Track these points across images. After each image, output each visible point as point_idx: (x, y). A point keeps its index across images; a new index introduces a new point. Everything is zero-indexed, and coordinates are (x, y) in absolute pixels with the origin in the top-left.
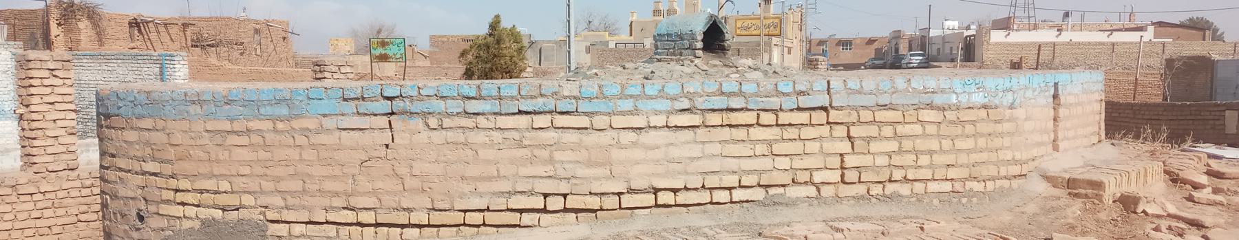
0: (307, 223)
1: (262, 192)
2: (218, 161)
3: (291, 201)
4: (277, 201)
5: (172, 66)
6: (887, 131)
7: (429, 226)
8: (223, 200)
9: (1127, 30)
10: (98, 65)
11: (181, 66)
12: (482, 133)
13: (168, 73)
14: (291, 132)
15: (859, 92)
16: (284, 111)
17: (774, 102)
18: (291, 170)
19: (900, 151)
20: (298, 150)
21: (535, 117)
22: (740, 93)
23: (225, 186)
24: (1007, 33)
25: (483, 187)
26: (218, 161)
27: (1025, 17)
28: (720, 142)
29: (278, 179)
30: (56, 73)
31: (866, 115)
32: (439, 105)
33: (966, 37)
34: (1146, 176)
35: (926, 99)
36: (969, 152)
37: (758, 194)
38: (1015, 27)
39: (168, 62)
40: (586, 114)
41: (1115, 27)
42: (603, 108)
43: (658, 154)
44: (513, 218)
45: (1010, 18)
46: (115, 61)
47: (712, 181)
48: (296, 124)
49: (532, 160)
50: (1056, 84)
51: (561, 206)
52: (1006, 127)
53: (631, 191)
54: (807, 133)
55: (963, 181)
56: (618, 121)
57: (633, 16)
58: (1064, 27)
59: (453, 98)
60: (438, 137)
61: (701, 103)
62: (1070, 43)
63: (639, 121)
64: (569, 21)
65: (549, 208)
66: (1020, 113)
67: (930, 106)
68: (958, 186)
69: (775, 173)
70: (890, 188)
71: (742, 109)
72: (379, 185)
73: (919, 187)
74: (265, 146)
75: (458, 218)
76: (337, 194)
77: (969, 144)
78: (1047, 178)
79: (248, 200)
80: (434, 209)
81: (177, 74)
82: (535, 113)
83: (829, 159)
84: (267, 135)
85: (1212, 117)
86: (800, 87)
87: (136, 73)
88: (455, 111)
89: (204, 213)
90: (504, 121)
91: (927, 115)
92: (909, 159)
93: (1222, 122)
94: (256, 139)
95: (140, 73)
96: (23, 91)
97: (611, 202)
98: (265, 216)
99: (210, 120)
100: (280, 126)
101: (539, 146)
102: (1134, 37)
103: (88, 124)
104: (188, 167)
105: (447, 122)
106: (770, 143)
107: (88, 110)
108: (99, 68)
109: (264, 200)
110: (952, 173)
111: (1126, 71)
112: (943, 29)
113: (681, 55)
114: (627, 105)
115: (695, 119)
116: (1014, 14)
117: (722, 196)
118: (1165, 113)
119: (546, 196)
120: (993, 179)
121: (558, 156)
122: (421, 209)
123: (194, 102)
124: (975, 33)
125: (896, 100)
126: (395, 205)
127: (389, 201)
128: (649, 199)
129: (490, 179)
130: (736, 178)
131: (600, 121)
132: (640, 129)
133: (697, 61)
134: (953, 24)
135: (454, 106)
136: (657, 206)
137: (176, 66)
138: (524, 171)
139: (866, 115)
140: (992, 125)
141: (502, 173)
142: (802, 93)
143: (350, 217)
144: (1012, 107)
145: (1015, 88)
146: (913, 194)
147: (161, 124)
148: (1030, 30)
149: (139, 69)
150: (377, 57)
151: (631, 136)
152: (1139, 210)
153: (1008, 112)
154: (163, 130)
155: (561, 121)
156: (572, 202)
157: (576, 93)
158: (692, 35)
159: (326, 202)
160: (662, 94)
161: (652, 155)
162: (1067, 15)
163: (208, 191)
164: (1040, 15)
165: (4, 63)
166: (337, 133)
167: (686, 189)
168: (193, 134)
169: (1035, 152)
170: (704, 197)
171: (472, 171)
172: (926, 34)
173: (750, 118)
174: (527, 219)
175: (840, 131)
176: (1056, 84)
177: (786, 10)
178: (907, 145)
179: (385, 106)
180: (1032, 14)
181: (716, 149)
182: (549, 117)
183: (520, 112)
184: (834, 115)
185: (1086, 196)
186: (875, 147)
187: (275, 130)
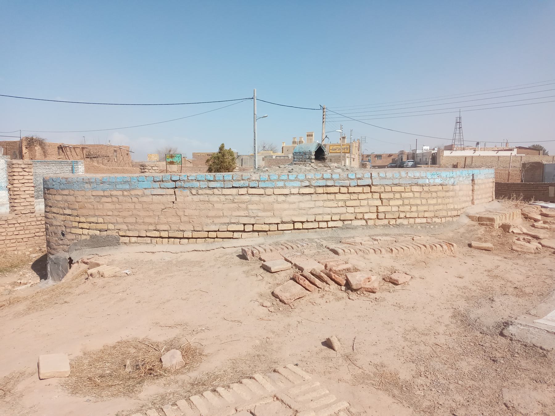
0: (137, 237)
1: (117, 223)
2: (98, 209)
3: (130, 227)
4: (124, 227)
5: (77, 167)
6: (398, 196)
7: (192, 238)
9: (505, 150)
11: (81, 166)
13: (75, 170)
16: (127, 187)
17: (347, 183)
18: (130, 213)
19: (403, 205)
20: (133, 204)
21: (240, 189)
22: (332, 179)
23: (101, 220)
25: (217, 221)
26: (98, 209)
28: (322, 201)
29: (124, 217)
30: (25, 170)
31: (388, 189)
32: (197, 184)
33: (433, 153)
35: (415, 181)
36: (434, 205)
37: (340, 224)
38: (455, 149)
40: (262, 188)
41: (499, 149)
42: (270, 185)
44: (230, 235)
45: (452, 145)
46: (51, 164)
48: (133, 192)
49: (239, 209)
52: (451, 194)
53: (283, 222)
54: (362, 196)
55: (432, 218)
56: (277, 191)
57: (283, 144)
58: (477, 149)
59: (203, 181)
60: (196, 198)
61: (314, 183)
62: (479, 156)
63: (286, 191)
64: (255, 147)
66: (457, 187)
67: (417, 184)
68: (429, 220)
69: (347, 214)
70: (399, 221)
72: (170, 220)
73: (412, 221)
74: (119, 203)
75: (205, 234)
76: (151, 224)
77: (434, 201)
79: (111, 226)
82: (240, 187)
83: (371, 208)
84: (120, 198)
86: (358, 176)
88: (204, 186)
89: (92, 232)
90: (226, 191)
91: (415, 188)
92: (407, 208)
95: (63, 170)
96: (11, 178)
100: (125, 193)
102: (508, 153)
103: (39, 192)
104: (84, 212)
105: (200, 192)
106: (345, 201)
107: (40, 186)
108: (44, 167)
109: (118, 227)
110: (426, 215)
111: (504, 169)
112: (422, 150)
114: (281, 184)
115: (311, 190)
118: (522, 188)
119: (244, 225)
120: (445, 217)
121: (250, 207)
122: (189, 231)
123: (87, 183)
124: (437, 152)
125: (401, 182)
126: (177, 229)
127: (174, 227)
129: (219, 217)
131: (269, 191)
132: (287, 195)
133: (312, 164)
135: (203, 185)
136: (294, 229)
137: (79, 167)
139: (388, 189)
140: (444, 193)
141: (225, 214)
142: (359, 179)
143: (157, 234)
144: (453, 185)
145: (455, 176)
147: (72, 192)
149: (62, 168)
151: (283, 198)
152: (510, 231)
153: (452, 187)
156: (256, 228)
157: (258, 179)
158: (310, 153)
159: (146, 227)
160: (297, 179)
161: (292, 206)
162: (478, 144)
163: (93, 223)
164: (466, 144)
166: (151, 197)
167: (307, 221)
168: (86, 197)
169: (464, 205)
170: (316, 225)
171: (212, 213)
173: (336, 190)
174: (236, 235)
175: (376, 196)
177: (352, 142)
178: (406, 202)
179: (173, 184)
180: (462, 143)
181: (321, 203)
182: (246, 189)
183: (233, 187)
184: (374, 189)
185: (487, 225)
186: (392, 203)
187: (123, 195)
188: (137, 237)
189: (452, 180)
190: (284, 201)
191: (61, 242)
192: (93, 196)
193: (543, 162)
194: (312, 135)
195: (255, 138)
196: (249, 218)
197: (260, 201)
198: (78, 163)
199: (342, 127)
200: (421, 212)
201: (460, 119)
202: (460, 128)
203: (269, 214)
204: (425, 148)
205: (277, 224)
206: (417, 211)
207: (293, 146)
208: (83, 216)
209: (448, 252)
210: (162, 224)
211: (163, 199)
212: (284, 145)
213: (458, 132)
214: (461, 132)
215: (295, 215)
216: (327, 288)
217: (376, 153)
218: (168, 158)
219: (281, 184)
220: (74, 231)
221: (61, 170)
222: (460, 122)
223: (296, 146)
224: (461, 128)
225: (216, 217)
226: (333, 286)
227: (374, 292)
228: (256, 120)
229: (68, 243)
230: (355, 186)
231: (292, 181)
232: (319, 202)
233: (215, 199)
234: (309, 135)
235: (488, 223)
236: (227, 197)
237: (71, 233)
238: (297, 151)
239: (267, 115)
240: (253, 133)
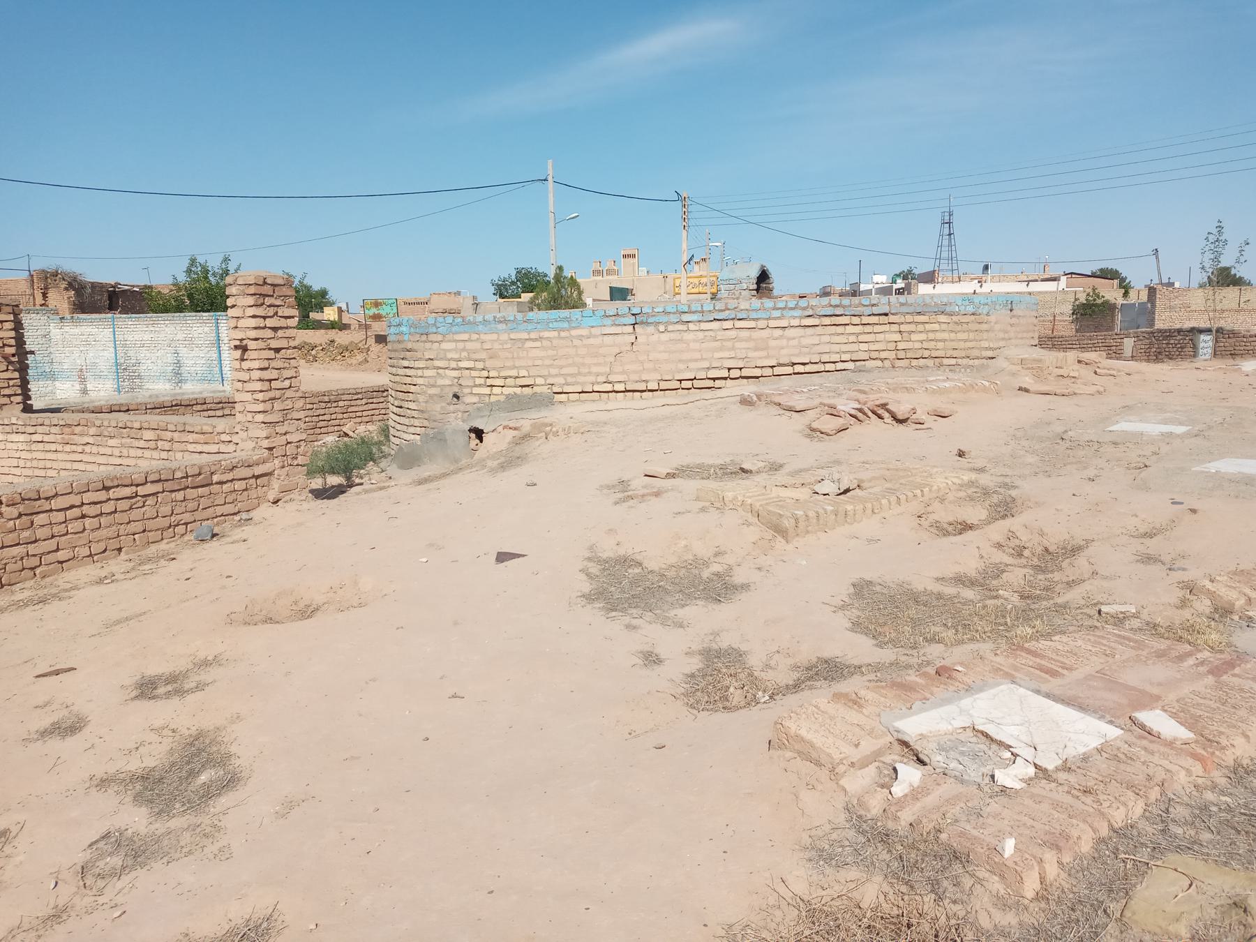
0: (580, 393)
1: (550, 375)
2: (519, 358)
3: (570, 380)
10: (145, 326)
14: (571, 338)
16: (566, 325)
24: (933, 285)
25: (692, 365)
27: (947, 270)
28: (829, 335)
29: (561, 367)
40: (754, 319)
41: (1030, 278)
43: (795, 342)
44: (710, 383)
46: (162, 322)
47: (825, 358)
48: (574, 333)
49: (721, 349)
52: (984, 327)
56: (773, 323)
58: (984, 279)
59: (674, 313)
60: (665, 337)
63: (784, 323)
69: (860, 353)
71: (841, 315)
72: (627, 367)
74: (554, 348)
79: (539, 381)
85: (1115, 344)
87: (185, 332)
89: (507, 391)
90: (704, 326)
91: (943, 318)
94: (546, 343)
98: (552, 390)
99: (512, 332)
100: (563, 334)
102: (1051, 286)
103: (135, 380)
105: (670, 328)
106: (858, 335)
107: (135, 368)
108: (147, 329)
109: (550, 381)
110: (955, 354)
114: (777, 314)
119: (729, 369)
121: (738, 345)
123: (501, 322)
129: (696, 360)
131: (762, 324)
136: (795, 374)
138: (717, 355)
143: (608, 387)
144: (988, 314)
145: (990, 303)
147: (475, 337)
148: (953, 282)
149: (188, 329)
150: (370, 317)
151: (778, 332)
156: (745, 373)
157: (748, 307)
159: (592, 379)
162: (986, 268)
163: (511, 377)
165: (43, 327)
166: (601, 338)
168: (500, 342)
171: (686, 356)
179: (632, 320)
181: (826, 339)
182: (731, 322)
186: (914, 337)
188: (580, 393)
190: (781, 337)
192: (512, 339)
196: (736, 360)
200: (948, 349)
201: (950, 215)
202: (950, 235)
204: (877, 278)
207: (595, 280)
208: (494, 369)
211: (619, 339)
213: (946, 242)
214: (953, 243)
218: (368, 307)
220: (476, 390)
221: (185, 332)
223: (600, 281)
229: (469, 408)
230: (869, 315)
231: (792, 309)
232: (825, 336)
236: (706, 333)
239: (577, 214)
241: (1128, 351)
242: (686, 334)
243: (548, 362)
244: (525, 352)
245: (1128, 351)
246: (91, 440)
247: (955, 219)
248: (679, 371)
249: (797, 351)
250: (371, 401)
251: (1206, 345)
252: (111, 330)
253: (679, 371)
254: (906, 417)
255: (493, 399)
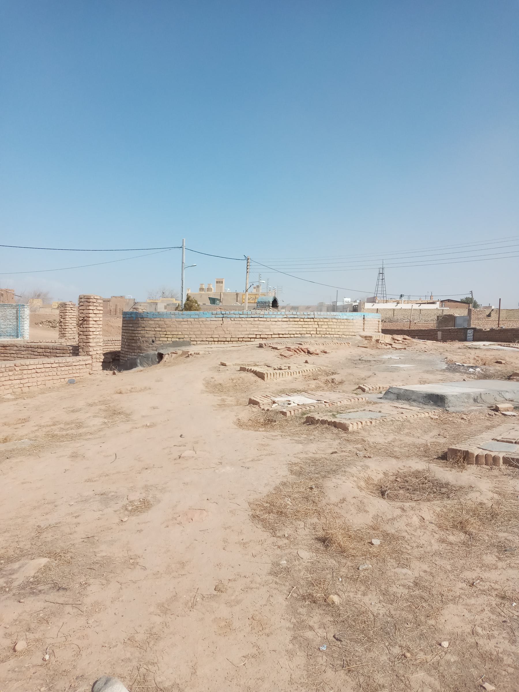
1: (190, 334)
2: (178, 328)
3: (197, 336)
4: (194, 336)
5: (23, 310)
6: (326, 323)
7: (231, 341)
8: (179, 336)
9: (428, 303)
11: (27, 310)
12: (243, 322)
13: (21, 313)
15: (320, 315)
16: (197, 317)
17: (303, 317)
18: (198, 330)
19: (328, 328)
20: (200, 325)
21: (255, 318)
22: (297, 315)
23: (180, 333)
25: (243, 333)
26: (178, 328)
29: (194, 332)
30: (72, 309)
31: (321, 320)
32: (234, 316)
33: (354, 306)
34: (385, 337)
35: (334, 317)
36: (343, 329)
37: (299, 336)
38: (377, 302)
39: (21, 308)
40: (265, 318)
42: (269, 317)
44: (249, 339)
45: (374, 297)
48: (200, 319)
50: (364, 316)
51: (259, 337)
52: (351, 324)
53: (274, 334)
54: (310, 323)
55: (341, 335)
56: (272, 320)
57: (188, 291)
58: (400, 302)
59: (237, 314)
61: (289, 316)
62: (401, 309)
63: (276, 320)
64: (182, 294)
65: (257, 337)
66: (355, 321)
67: (335, 318)
68: (340, 336)
69: (303, 331)
70: (326, 335)
72: (219, 332)
73: (332, 336)
75: (237, 339)
76: (209, 335)
77: (342, 327)
78: (361, 336)
80: (232, 338)
81: (25, 313)
82: (255, 318)
83: (314, 329)
84: (192, 322)
86: (308, 314)
88: (237, 317)
90: (248, 319)
91: (334, 320)
92: (330, 330)
93: (436, 336)
95: (5, 312)
96: (62, 314)
97: (270, 336)
101: (255, 324)
104: (170, 329)
105: (236, 319)
106: (302, 325)
110: (339, 333)
111: (426, 322)
112: (343, 302)
113: (265, 308)
114: (273, 316)
115: (288, 320)
116: (377, 295)
117: (292, 336)
118: (419, 333)
119: (256, 335)
120: (348, 335)
121: (259, 326)
122: (229, 338)
123: (173, 314)
124: (358, 304)
125: (328, 317)
126: (223, 337)
127: (221, 336)
128: (278, 336)
129: (244, 331)
130: (295, 332)
131: (268, 320)
133: (270, 310)
134: (348, 300)
135: (237, 316)
136: (279, 337)
137: (25, 310)
139: (321, 320)
140: (348, 323)
141: (247, 330)
142: (309, 315)
143: (212, 339)
144: (353, 320)
145: (353, 315)
146: (331, 337)
147: (162, 319)
152: (379, 342)
153: (352, 321)
154: (163, 321)
155: (260, 319)
156: (262, 336)
158: (269, 302)
159: (206, 336)
160: (281, 314)
161: (279, 327)
162: (401, 296)
163: (175, 335)
164: (388, 297)
166: (210, 321)
167: (285, 334)
169: (358, 330)
170: (289, 336)
171: (240, 329)
172: (335, 304)
174: (252, 340)
175: (316, 323)
176: (364, 316)
177: (268, 291)
178: (330, 326)
179: (222, 316)
180: (385, 295)
181: (291, 326)
182: (258, 318)
183: (252, 317)
184: (315, 320)
185: (369, 339)
186: (323, 327)
187: (194, 321)
189: (352, 317)
191: (151, 346)
193: (455, 314)
194: (222, 282)
195: (182, 285)
197: (264, 324)
198: (24, 306)
199: (260, 276)
200: (336, 331)
201: (383, 270)
202: (382, 279)
203: (269, 330)
205: (271, 335)
206: (335, 331)
209: (347, 346)
210: (215, 334)
212: (189, 292)
213: (380, 283)
215: (279, 331)
216: (300, 353)
217: (292, 304)
219: (273, 316)
220: (161, 339)
222: (382, 274)
223: (203, 294)
224: (384, 280)
225: (242, 331)
226: (303, 353)
227: (318, 355)
228: (184, 268)
229: (157, 346)
233: (243, 322)
234: (219, 282)
235: (369, 338)
236: (248, 322)
237: (159, 340)
238: (260, 301)
240: (181, 282)
241: (439, 337)
242: (241, 322)
243: (189, 329)
244: (181, 326)
245: (439, 337)
246: (14, 352)
247: (385, 271)
248: (238, 335)
249: (280, 330)
250: (107, 345)
251: (470, 335)
252: (15, 311)
253: (238, 335)
254: (313, 352)
255: (168, 342)
